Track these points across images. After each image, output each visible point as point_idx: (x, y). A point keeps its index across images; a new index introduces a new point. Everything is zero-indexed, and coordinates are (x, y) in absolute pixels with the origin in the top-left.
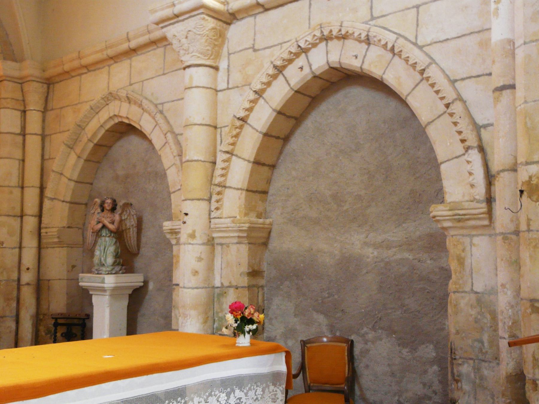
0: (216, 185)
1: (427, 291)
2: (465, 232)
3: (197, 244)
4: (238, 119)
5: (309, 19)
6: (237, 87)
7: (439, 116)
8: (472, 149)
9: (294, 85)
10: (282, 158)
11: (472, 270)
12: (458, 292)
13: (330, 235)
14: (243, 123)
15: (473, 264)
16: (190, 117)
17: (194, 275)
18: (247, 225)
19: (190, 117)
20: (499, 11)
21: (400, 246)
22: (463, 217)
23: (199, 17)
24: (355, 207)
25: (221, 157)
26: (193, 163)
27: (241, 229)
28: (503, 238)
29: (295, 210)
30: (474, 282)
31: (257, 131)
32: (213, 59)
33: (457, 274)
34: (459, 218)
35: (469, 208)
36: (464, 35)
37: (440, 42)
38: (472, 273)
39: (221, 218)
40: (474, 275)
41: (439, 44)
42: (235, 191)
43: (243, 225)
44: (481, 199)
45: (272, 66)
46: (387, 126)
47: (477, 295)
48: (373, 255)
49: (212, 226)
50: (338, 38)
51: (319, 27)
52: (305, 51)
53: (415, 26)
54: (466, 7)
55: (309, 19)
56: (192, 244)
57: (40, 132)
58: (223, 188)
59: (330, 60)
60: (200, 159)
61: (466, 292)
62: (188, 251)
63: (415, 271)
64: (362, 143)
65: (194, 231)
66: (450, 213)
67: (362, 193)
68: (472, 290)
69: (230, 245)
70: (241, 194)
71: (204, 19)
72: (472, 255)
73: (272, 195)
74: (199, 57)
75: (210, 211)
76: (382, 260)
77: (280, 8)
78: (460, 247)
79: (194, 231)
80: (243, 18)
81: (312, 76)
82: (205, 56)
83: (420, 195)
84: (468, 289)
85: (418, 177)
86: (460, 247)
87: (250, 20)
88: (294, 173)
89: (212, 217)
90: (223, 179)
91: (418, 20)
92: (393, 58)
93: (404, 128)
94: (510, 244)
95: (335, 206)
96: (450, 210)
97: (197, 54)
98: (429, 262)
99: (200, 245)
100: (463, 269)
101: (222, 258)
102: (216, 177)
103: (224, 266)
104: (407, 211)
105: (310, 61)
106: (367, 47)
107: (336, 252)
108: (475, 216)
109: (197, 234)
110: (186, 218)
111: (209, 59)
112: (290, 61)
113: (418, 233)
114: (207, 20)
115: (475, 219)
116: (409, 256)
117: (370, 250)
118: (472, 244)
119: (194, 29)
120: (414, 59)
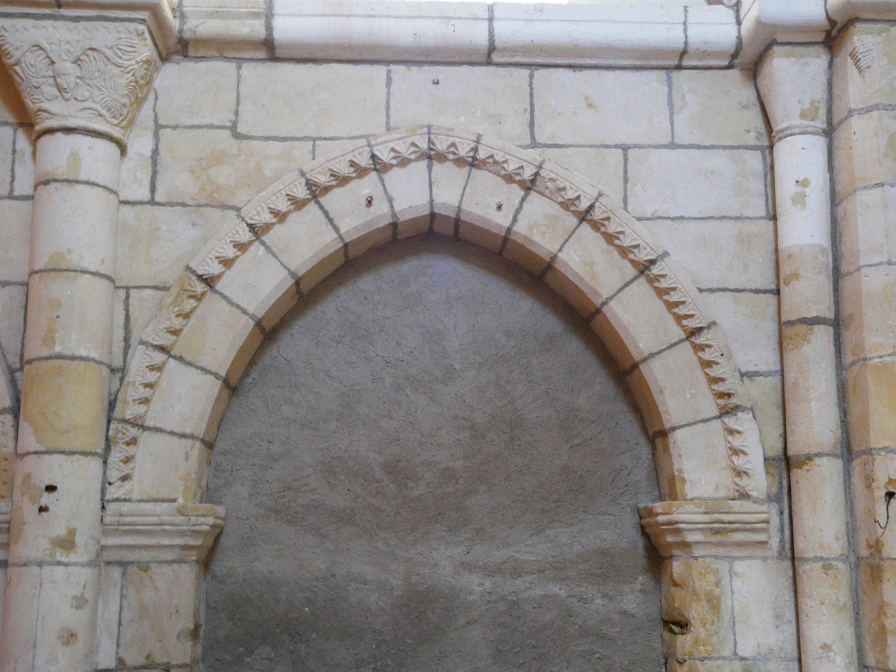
0: (124, 421)
1: (597, 655)
2: (721, 551)
3: (75, 564)
4: (200, 277)
5: (388, 108)
6: (183, 205)
7: (671, 347)
8: (743, 411)
9: (348, 232)
10: (254, 374)
11: (734, 618)
12: (710, 659)
13: (380, 545)
14: (208, 288)
15: (736, 608)
16: (70, 251)
17: (67, 644)
18: (211, 520)
19: (70, 251)
20: (807, 199)
21: (541, 571)
22: (727, 526)
23: (131, 26)
24: (439, 491)
25: (140, 359)
26: (75, 363)
27: (197, 528)
28: (823, 567)
29: (289, 488)
30: (737, 639)
31: (244, 312)
32: (123, 128)
33: (708, 626)
34: (720, 528)
35: (741, 511)
36: (711, 218)
37: (668, 218)
38: (734, 623)
39: (129, 500)
40: (737, 628)
41: (668, 222)
42: (176, 441)
43: (202, 519)
44: (761, 497)
45: (303, 181)
46: (512, 343)
47: (744, 662)
48: (481, 589)
49: (108, 520)
50: (460, 162)
51: (425, 130)
52: (379, 167)
53: (622, 180)
54: (713, 173)
55: (388, 108)
56: (66, 565)
57: (830, 315)
58: (141, 431)
59: (438, 200)
60: (92, 356)
61: (724, 658)
62: (54, 582)
63: (572, 619)
64: (457, 367)
65: (72, 532)
66: (706, 518)
67: (459, 465)
68: (735, 653)
69: (153, 566)
70: (193, 446)
71: (140, 35)
72: (733, 593)
73: (225, 453)
74: (101, 115)
75: (106, 483)
76: (503, 598)
77: (310, 65)
78: (711, 578)
79: (72, 532)
80: (203, 58)
81: (390, 221)
82: (114, 117)
83: (581, 476)
84: (727, 652)
85: (578, 445)
86: (711, 578)
87: (226, 69)
88: (287, 410)
89: (107, 497)
90: (142, 409)
91: (626, 172)
92: (578, 226)
93: (548, 351)
94: (836, 577)
95: (393, 487)
96: (705, 513)
97: (99, 107)
98: (599, 601)
99: (83, 566)
100: (718, 617)
101: (122, 597)
102: (126, 402)
103: (127, 616)
104: (554, 505)
105: (389, 191)
106: (523, 193)
107: (395, 582)
108: (748, 526)
109: (79, 540)
110: (47, 499)
111: (117, 125)
112: (343, 181)
113: (577, 548)
114: (145, 39)
115: (746, 530)
116: (558, 590)
117: (475, 579)
118: (732, 573)
119: (111, 48)
120: (635, 239)
